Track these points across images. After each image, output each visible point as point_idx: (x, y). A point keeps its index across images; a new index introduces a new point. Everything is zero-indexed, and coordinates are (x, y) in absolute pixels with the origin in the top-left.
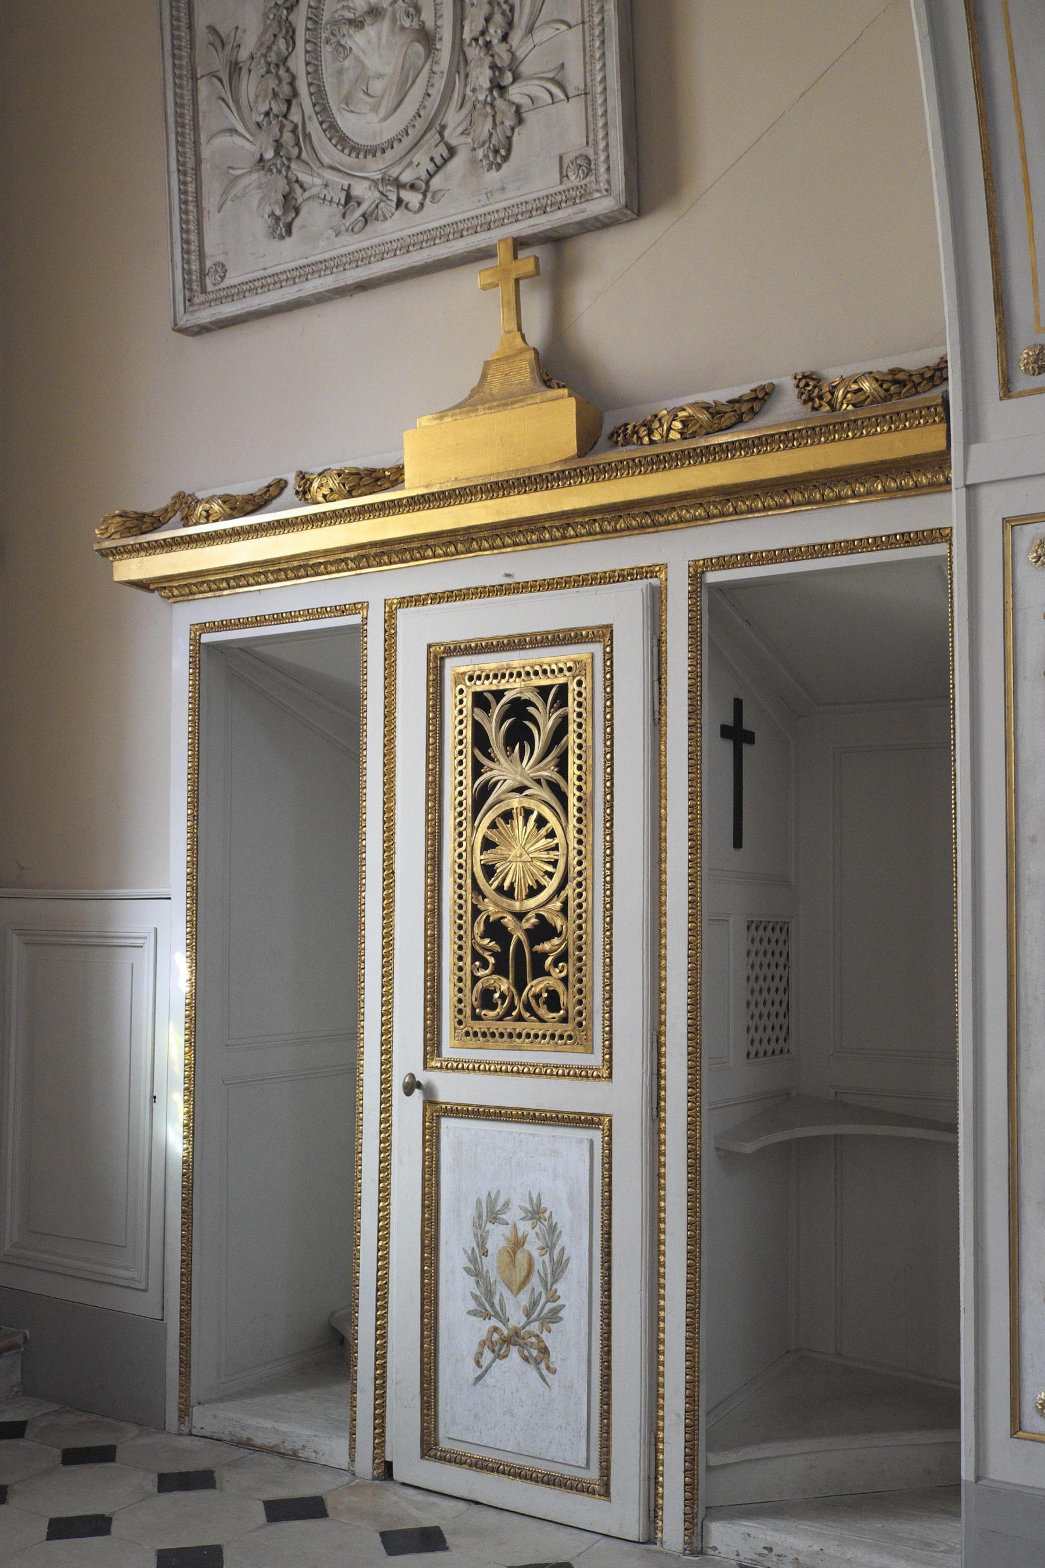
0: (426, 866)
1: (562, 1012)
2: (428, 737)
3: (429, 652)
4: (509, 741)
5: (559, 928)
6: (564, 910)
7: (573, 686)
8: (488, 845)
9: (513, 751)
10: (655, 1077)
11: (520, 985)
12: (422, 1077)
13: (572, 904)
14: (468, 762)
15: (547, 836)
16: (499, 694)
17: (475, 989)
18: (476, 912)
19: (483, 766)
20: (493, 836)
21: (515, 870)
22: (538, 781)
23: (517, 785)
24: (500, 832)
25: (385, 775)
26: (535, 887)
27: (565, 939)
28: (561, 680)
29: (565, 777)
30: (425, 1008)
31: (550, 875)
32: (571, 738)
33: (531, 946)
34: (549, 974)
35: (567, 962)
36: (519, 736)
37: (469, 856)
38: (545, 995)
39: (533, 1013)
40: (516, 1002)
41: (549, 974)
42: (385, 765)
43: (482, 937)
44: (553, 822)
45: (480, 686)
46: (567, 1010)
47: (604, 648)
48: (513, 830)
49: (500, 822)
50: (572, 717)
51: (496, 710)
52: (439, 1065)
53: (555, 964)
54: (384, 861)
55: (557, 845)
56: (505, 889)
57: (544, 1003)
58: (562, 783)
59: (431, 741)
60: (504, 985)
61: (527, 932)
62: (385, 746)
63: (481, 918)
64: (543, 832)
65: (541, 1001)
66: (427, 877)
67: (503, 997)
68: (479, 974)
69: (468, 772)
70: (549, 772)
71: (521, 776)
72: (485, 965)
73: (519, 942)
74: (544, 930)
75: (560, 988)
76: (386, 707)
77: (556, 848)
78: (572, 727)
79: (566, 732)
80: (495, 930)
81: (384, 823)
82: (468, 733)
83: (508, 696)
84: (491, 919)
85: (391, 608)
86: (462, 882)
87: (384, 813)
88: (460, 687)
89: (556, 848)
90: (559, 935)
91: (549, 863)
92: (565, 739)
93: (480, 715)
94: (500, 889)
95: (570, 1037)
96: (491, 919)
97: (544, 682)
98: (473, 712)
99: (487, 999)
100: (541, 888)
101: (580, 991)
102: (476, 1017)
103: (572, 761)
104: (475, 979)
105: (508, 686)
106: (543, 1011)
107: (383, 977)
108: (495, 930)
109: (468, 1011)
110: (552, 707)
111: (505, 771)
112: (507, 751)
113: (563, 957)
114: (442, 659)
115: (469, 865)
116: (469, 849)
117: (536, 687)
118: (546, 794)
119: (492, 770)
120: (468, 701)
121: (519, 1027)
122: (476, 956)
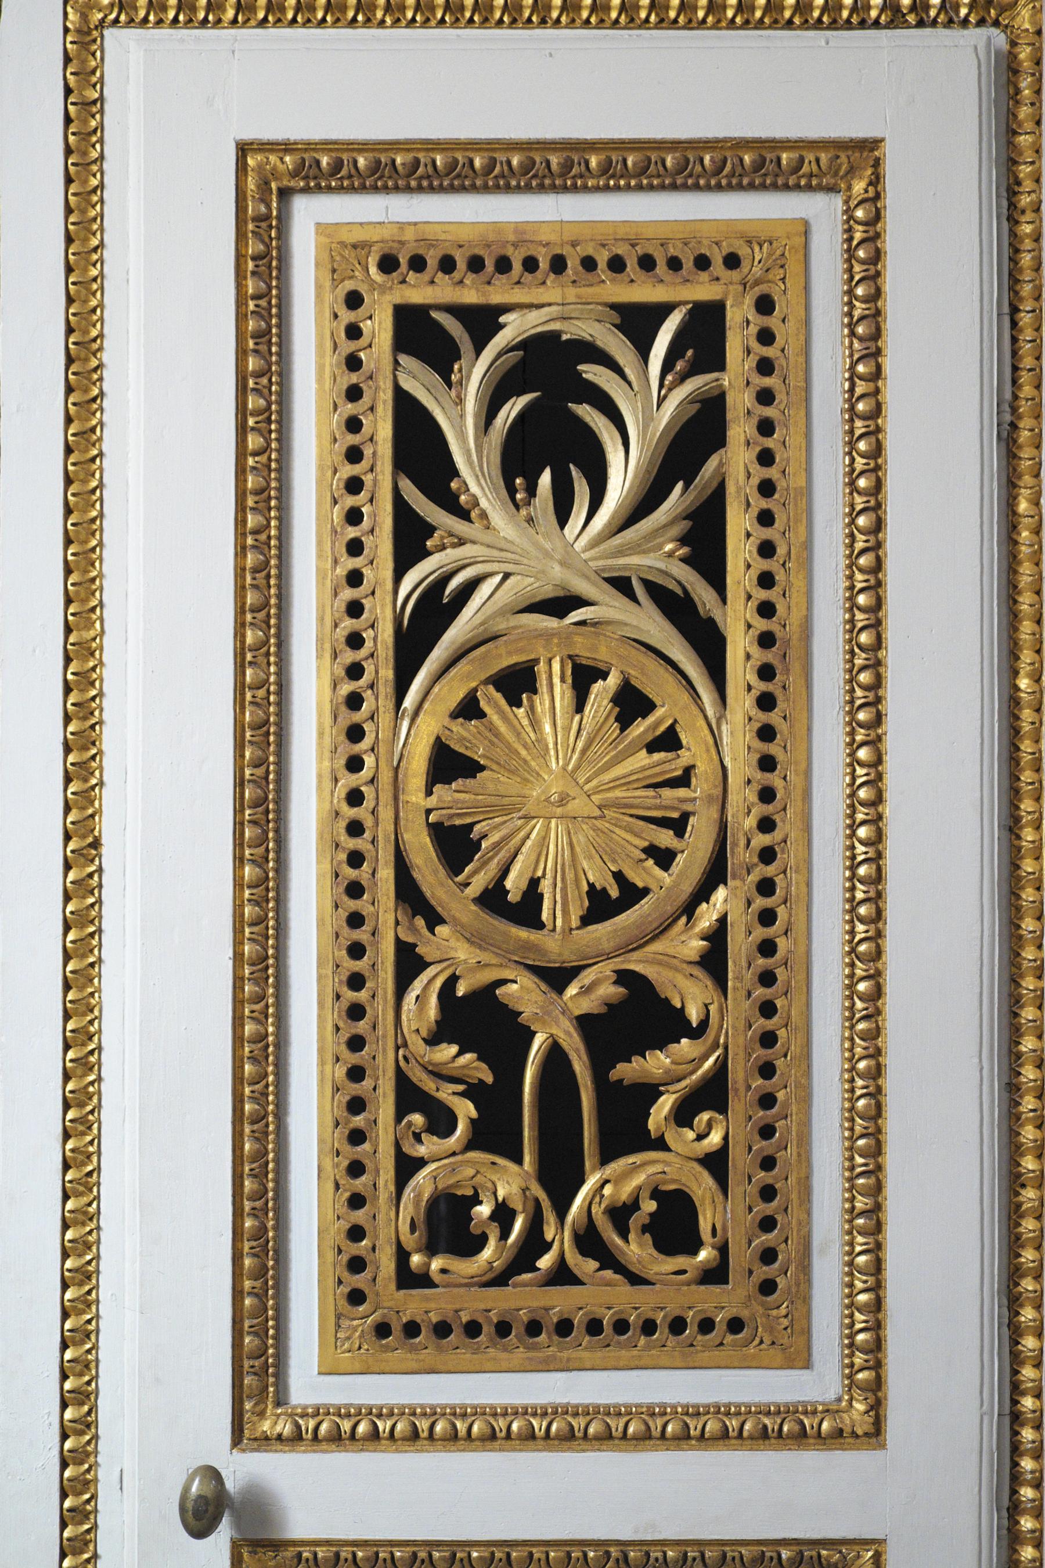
0: (239, 826)
1: (703, 1255)
2: (242, 430)
3: (241, 168)
4: (518, 463)
5: (694, 1015)
6: (714, 960)
7: (739, 314)
8: (448, 765)
9: (532, 490)
10: (1007, 1420)
11: (560, 1177)
12: (240, 1470)
13: (740, 944)
14: (381, 518)
15: (653, 747)
16: (483, 322)
17: (408, 1193)
18: (409, 964)
19: (430, 530)
20: (465, 737)
21: (544, 839)
22: (622, 585)
23: (548, 592)
24: (492, 728)
25: (68, 541)
26: (614, 893)
27: (715, 1046)
28: (703, 290)
29: (717, 580)
30: (237, 1258)
31: (664, 858)
32: (736, 461)
33: (600, 1068)
34: (660, 1144)
35: (722, 1108)
36: (552, 447)
37: (386, 796)
38: (650, 1206)
39: (608, 1260)
40: (549, 1233)
41: (660, 1144)
42: (68, 511)
43: (433, 1040)
44: (669, 706)
45: (418, 292)
46: (723, 1250)
47: (849, 212)
48: (535, 723)
49: (492, 701)
50: (740, 402)
51: (477, 373)
52: (288, 1430)
53: (683, 1115)
54: (67, 809)
55: (688, 770)
56: (513, 897)
57: (645, 1229)
58: (703, 594)
59: (253, 441)
60: (510, 1181)
61: (585, 1023)
62: (68, 450)
63: (426, 987)
64: (640, 728)
65: (636, 1221)
66: (239, 860)
67: (503, 1215)
68: (422, 1151)
69: (382, 545)
70: (661, 556)
71: (563, 564)
72: (441, 1122)
73: (555, 1054)
74: (641, 1017)
75: (701, 1186)
76: (70, 330)
77: (684, 780)
78: (740, 430)
79: (719, 441)
80: (478, 1020)
81: (68, 689)
82: (381, 428)
83: (514, 327)
84: (461, 991)
85: (84, 17)
86: (362, 874)
87: (68, 660)
88: (349, 285)
89: (684, 780)
90: (697, 1033)
91: (663, 823)
92: (711, 465)
93: (419, 381)
94: (493, 899)
95: (735, 1325)
96: (461, 991)
97: (644, 292)
98: (396, 363)
99: (450, 1224)
100: (632, 894)
101: (768, 1193)
102: (409, 1279)
103: (739, 524)
104: (407, 1167)
105: (518, 296)
106: (636, 1250)
107: (66, 1166)
108: (478, 1020)
109: (386, 1264)
110: (667, 367)
111: (510, 549)
112: (512, 491)
113: (711, 1094)
114: (285, 194)
115: (386, 826)
116: (385, 777)
117: (614, 307)
118: (651, 624)
119: (461, 542)
120: (380, 328)
121: (561, 1301)
122: (409, 1097)
